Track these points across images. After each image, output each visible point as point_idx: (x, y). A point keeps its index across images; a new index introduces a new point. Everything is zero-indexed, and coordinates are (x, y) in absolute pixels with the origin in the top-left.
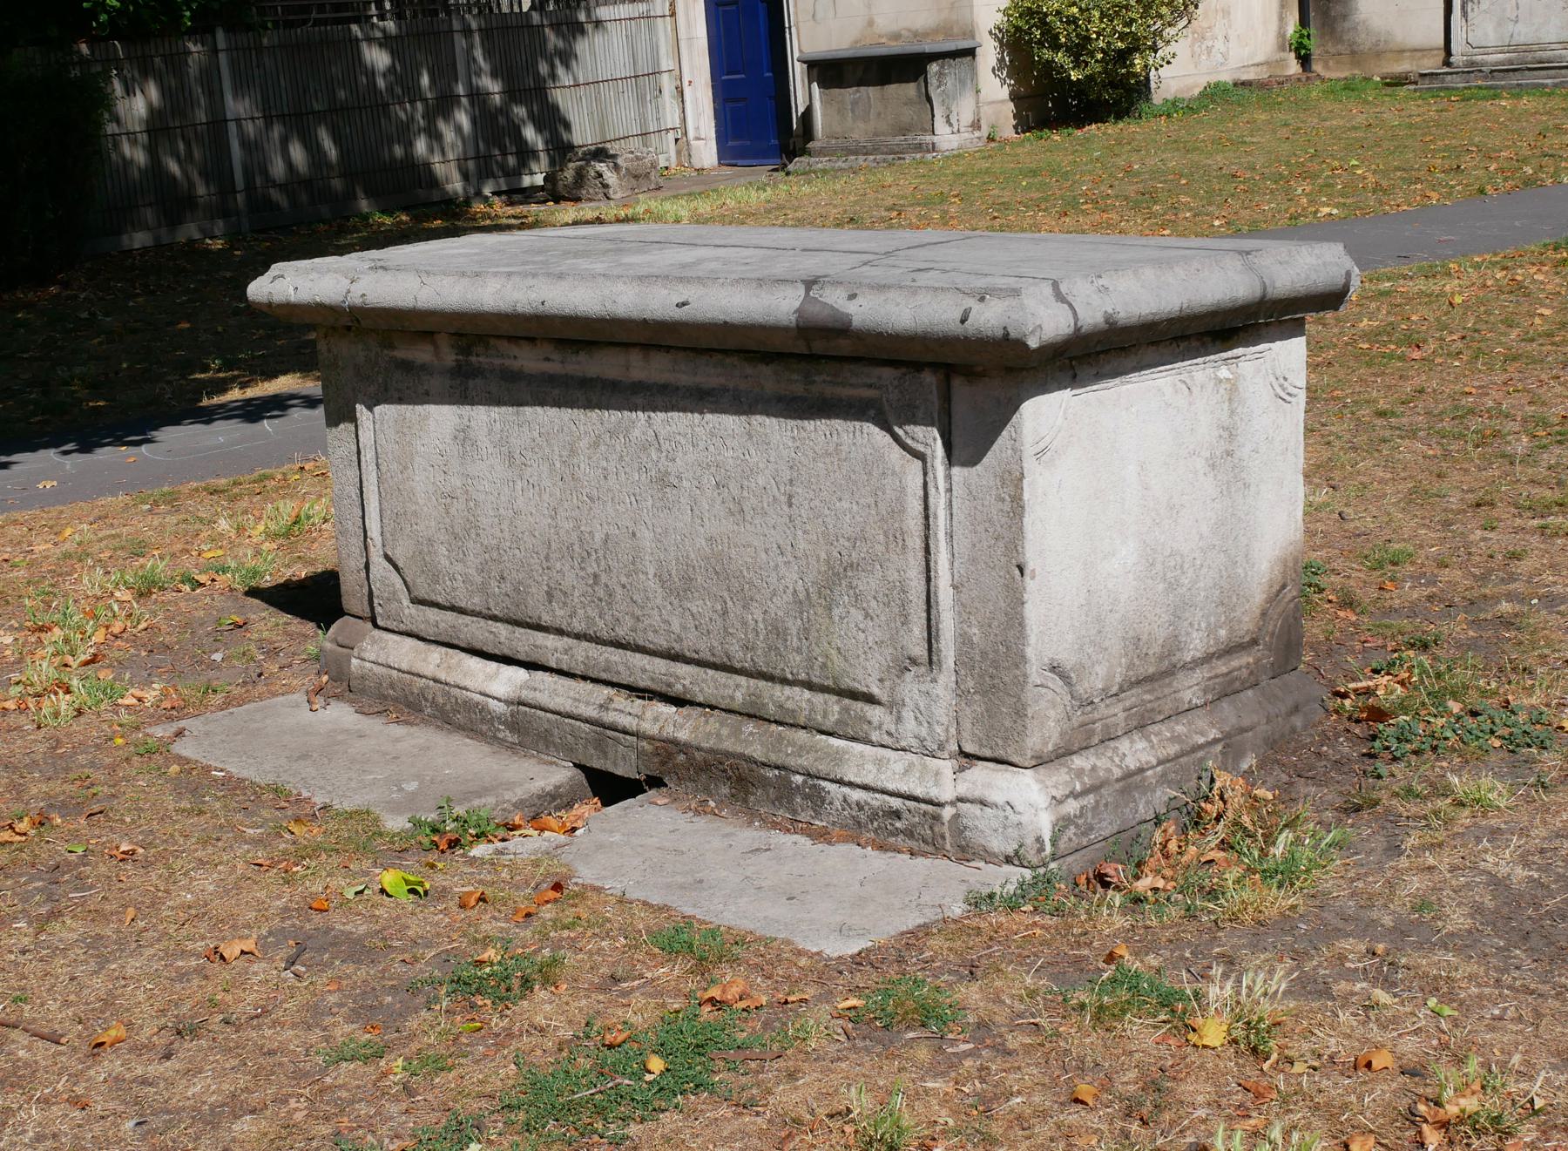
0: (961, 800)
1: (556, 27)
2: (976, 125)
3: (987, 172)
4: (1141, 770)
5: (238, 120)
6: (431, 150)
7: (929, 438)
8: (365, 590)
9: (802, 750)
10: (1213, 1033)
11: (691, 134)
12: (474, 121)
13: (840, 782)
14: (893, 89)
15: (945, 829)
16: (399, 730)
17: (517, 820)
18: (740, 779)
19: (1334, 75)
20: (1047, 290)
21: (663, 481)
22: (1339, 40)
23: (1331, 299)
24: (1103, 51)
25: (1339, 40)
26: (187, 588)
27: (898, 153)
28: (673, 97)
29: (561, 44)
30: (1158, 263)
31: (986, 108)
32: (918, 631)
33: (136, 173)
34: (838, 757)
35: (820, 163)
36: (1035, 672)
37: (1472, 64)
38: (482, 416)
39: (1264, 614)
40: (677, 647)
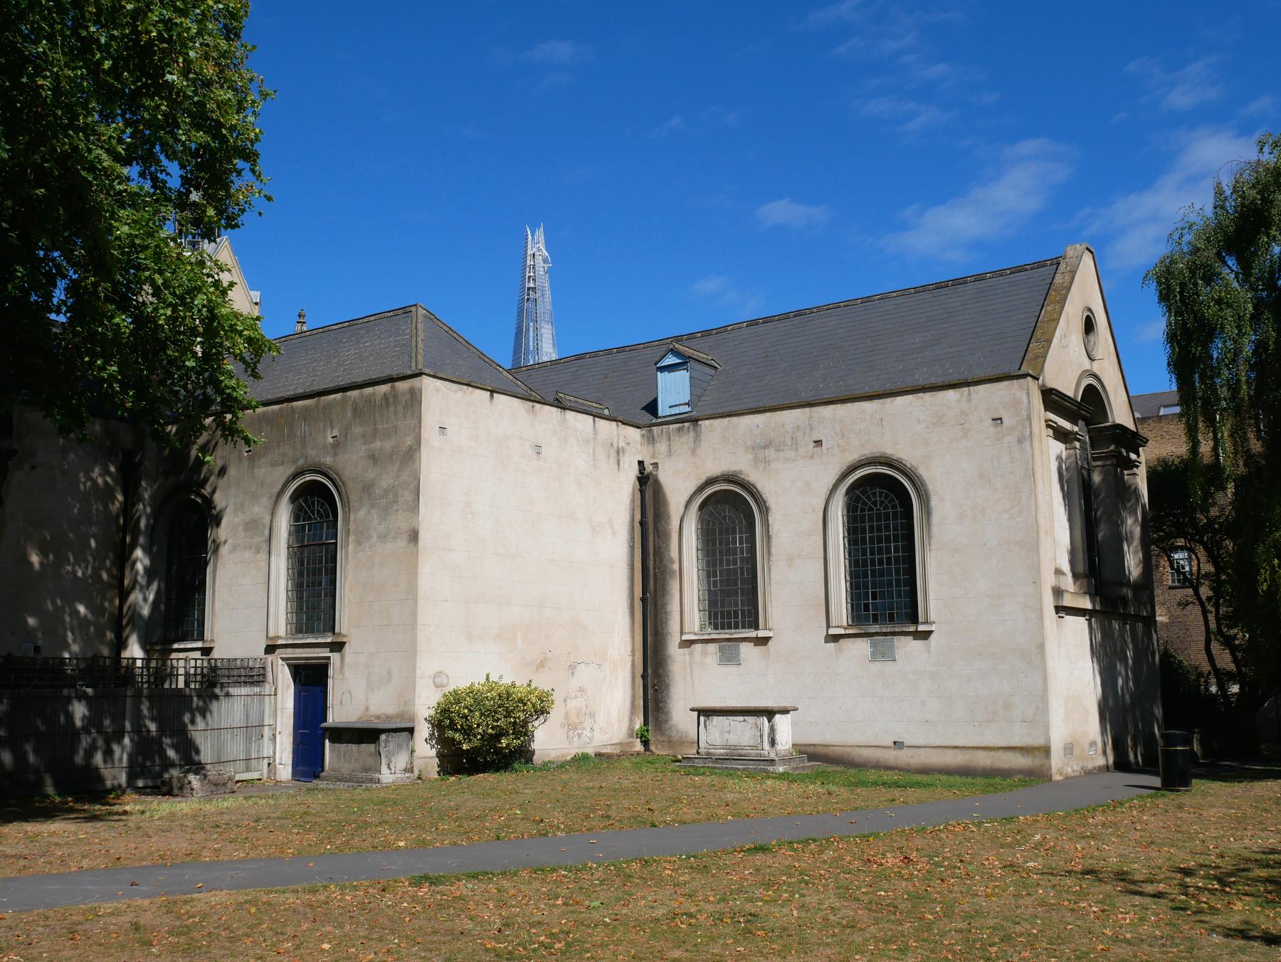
11: (277, 761)
22: (663, 734)
25: (663, 734)
27: (360, 782)
28: (270, 740)
31: (418, 760)
37: (709, 754)
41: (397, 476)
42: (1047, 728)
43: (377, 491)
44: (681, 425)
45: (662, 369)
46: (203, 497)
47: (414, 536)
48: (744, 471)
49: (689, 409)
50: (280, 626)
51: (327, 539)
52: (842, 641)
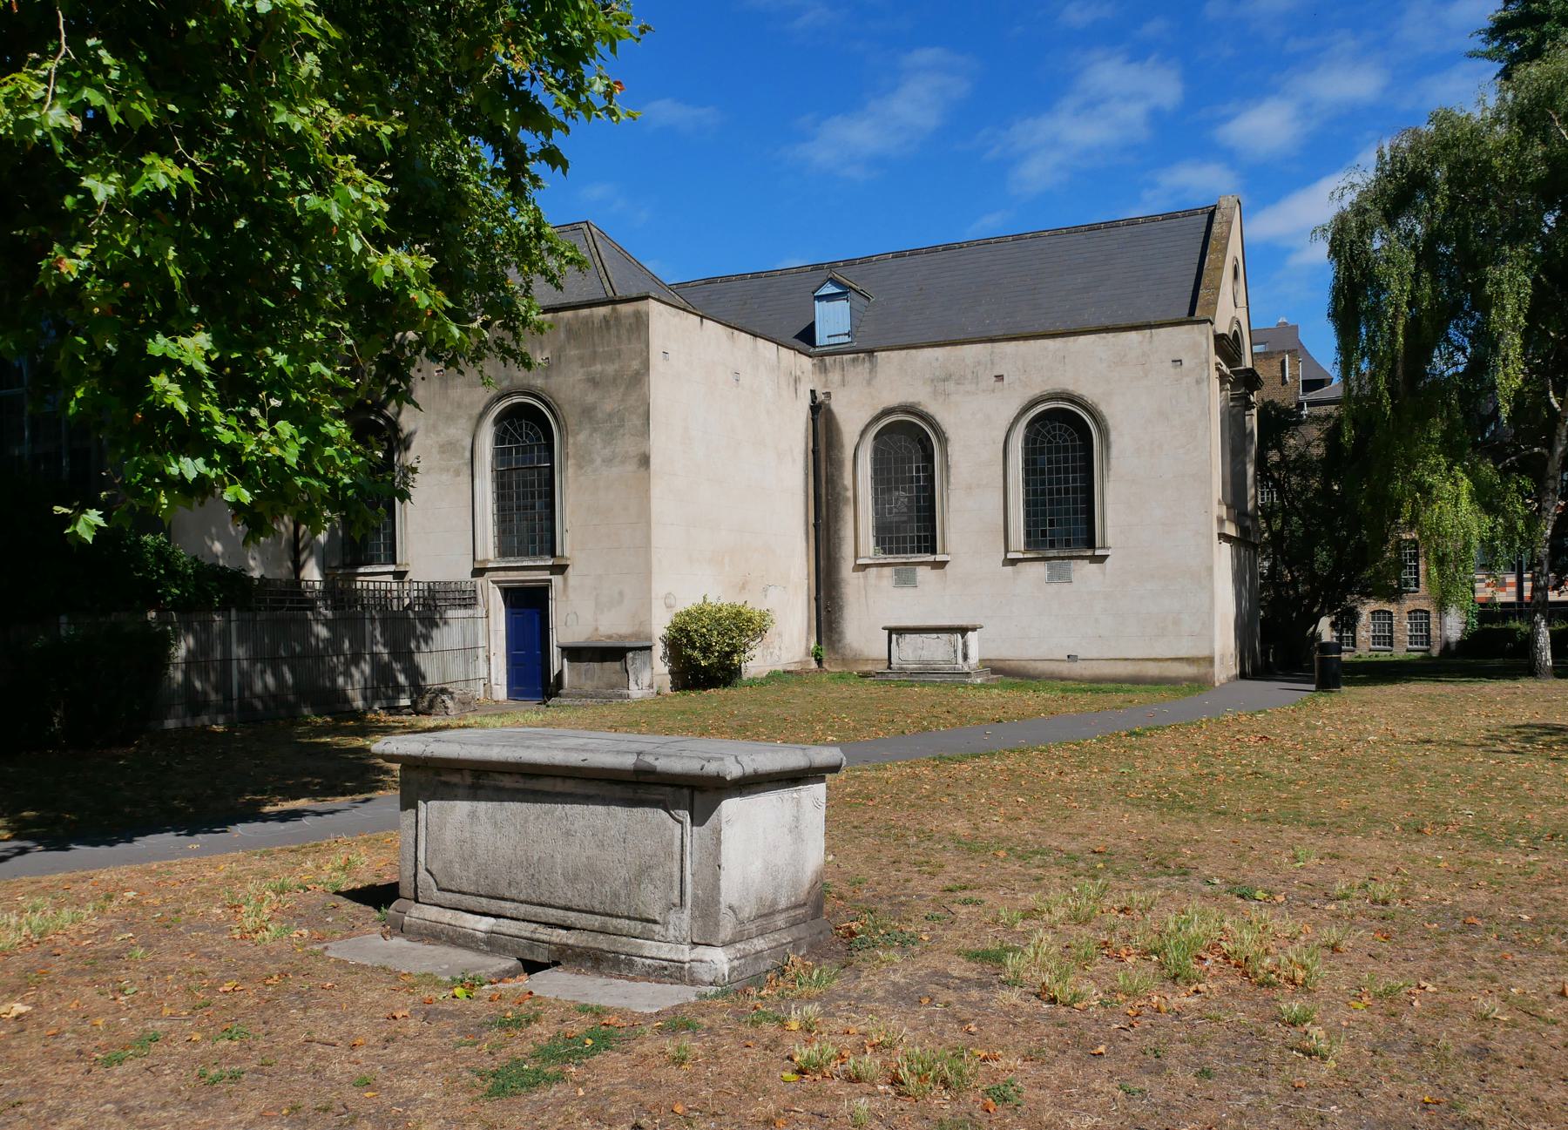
0: (692, 961)
1: (422, 621)
2: (651, 686)
3: (658, 711)
4: (762, 951)
5: (238, 660)
6: (346, 683)
7: (685, 815)
8: (413, 886)
9: (624, 945)
10: (794, 1026)
11: (493, 682)
12: (372, 669)
13: (642, 957)
14: (607, 664)
15: (686, 973)
16: (431, 947)
17: (493, 980)
18: (597, 959)
19: (835, 670)
20: (733, 758)
21: (568, 833)
22: (837, 653)
23: (835, 769)
24: (718, 651)
25: (837, 653)
26: (302, 891)
27: (609, 698)
29: (424, 631)
30: (772, 751)
32: (677, 892)
33: (176, 685)
34: (640, 947)
35: (566, 701)
36: (723, 908)
37: (902, 669)
38: (483, 807)
39: (809, 893)
40: (569, 904)
41: (623, 400)
42: (1212, 640)
43: (600, 415)
44: (855, 355)
45: (821, 298)
46: (387, 419)
47: (645, 461)
48: (923, 403)
49: (850, 340)
50: (488, 549)
51: (539, 462)
52: (1019, 565)
